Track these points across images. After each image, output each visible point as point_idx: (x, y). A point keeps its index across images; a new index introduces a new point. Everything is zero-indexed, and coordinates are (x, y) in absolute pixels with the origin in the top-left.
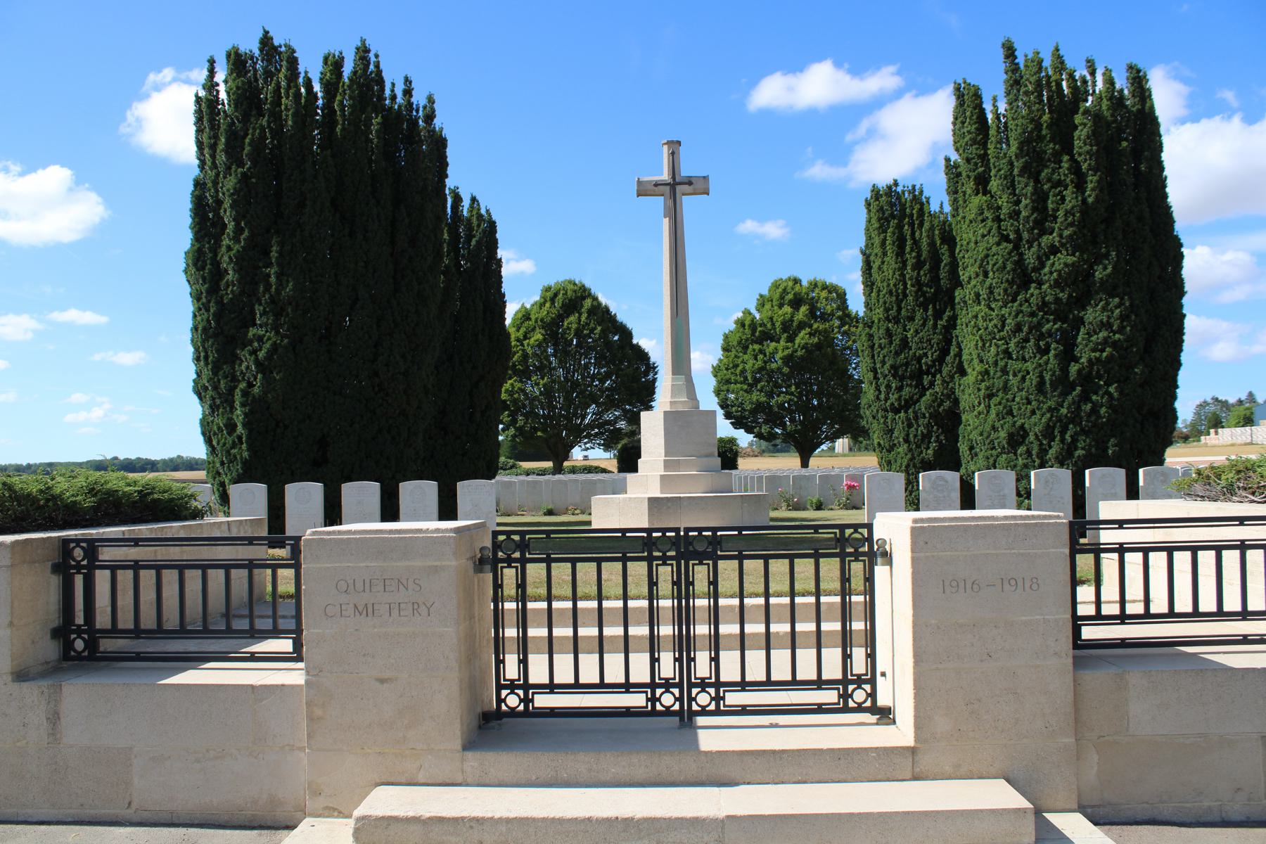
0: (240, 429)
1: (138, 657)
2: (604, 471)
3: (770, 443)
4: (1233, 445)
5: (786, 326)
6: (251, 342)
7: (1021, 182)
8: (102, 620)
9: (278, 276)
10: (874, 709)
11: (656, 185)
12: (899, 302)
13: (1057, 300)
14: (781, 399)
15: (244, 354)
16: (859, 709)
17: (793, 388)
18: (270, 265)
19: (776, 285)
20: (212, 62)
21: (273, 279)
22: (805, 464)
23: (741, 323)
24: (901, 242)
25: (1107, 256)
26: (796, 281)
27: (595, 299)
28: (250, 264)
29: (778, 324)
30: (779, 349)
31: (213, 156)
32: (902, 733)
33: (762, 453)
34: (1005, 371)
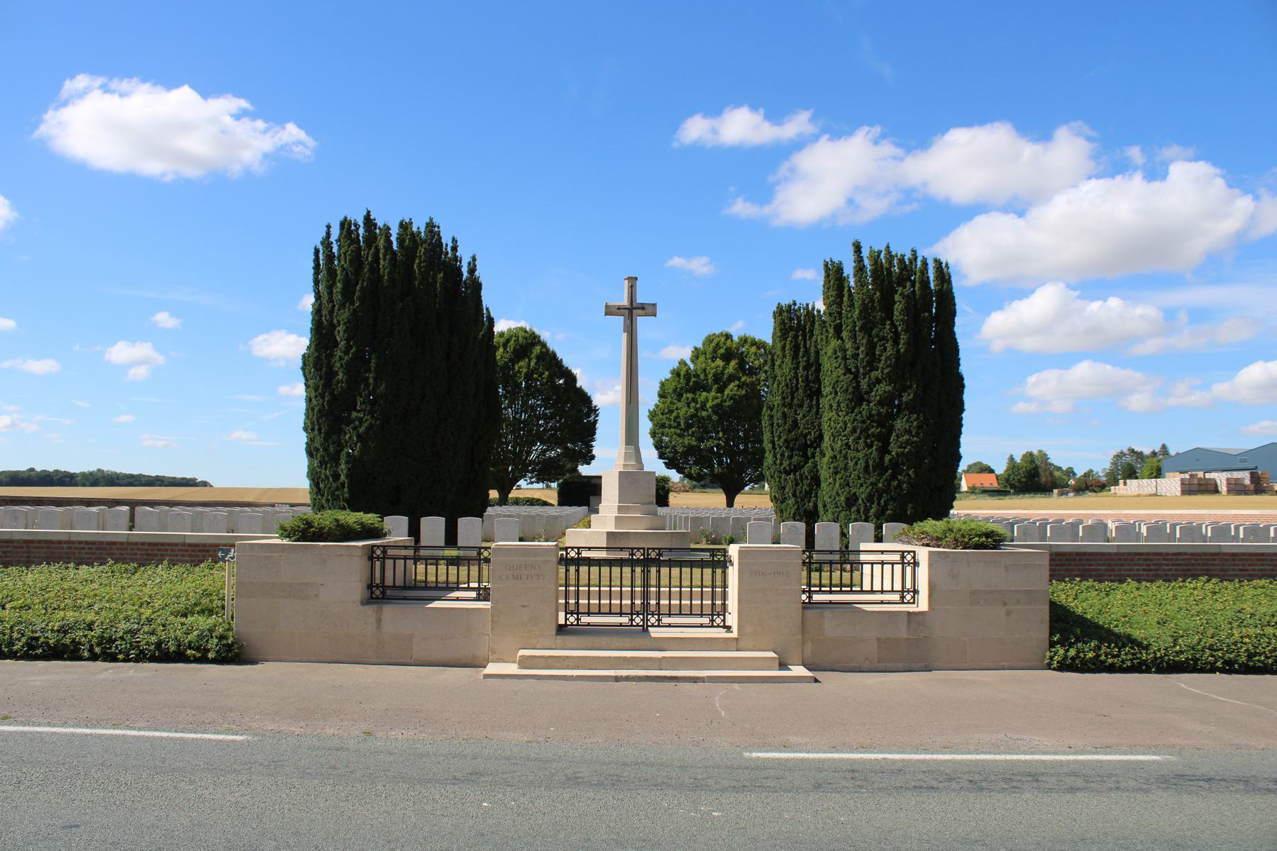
0: (343, 477)
1: (405, 598)
2: (545, 504)
3: (700, 481)
4: (1138, 496)
5: (717, 378)
6: (353, 421)
7: (860, 335)
8: (389, 582)
9: (375, 379)
10: (724, 627)
11: (619, 308)
12: (792, 393)
13: (879, 414)
14: (710, 443)
15: (349, 429)
16: (718, 626)
17: (721, 434)
18: (369, 371)
19: (709, 340)
20: (329, 227)
21: (371, 381)
22: (730, 503)
23: (676, 373)
24: (796, 348)
25: (911, 386)
26: (728, 337)
27: (544, 345)
28: (356, 368)
29: (710, 376)
30: (710, 398)
31: (330, 293)
32: (735, 634)
33: (693, 489)
34: (845, 457)
